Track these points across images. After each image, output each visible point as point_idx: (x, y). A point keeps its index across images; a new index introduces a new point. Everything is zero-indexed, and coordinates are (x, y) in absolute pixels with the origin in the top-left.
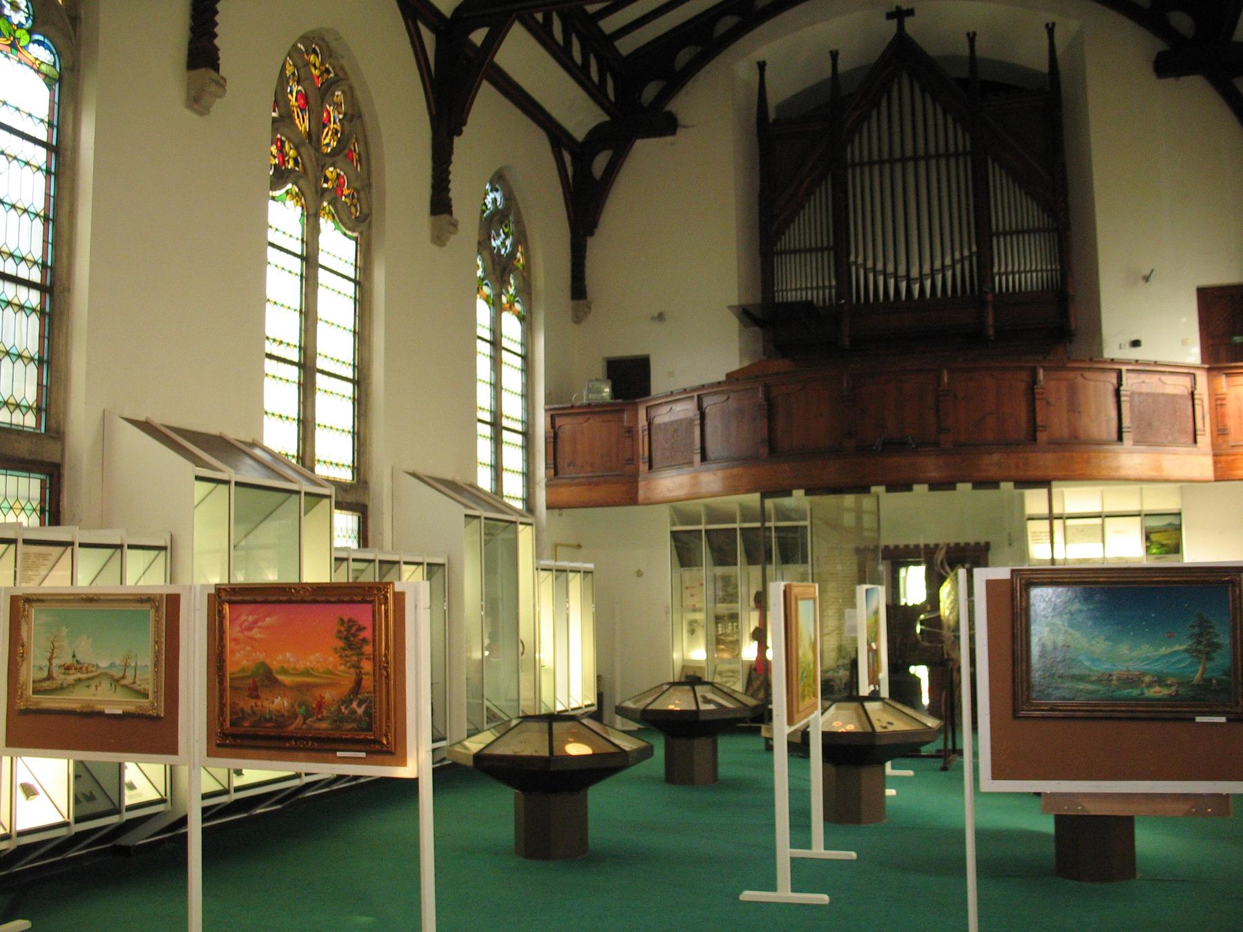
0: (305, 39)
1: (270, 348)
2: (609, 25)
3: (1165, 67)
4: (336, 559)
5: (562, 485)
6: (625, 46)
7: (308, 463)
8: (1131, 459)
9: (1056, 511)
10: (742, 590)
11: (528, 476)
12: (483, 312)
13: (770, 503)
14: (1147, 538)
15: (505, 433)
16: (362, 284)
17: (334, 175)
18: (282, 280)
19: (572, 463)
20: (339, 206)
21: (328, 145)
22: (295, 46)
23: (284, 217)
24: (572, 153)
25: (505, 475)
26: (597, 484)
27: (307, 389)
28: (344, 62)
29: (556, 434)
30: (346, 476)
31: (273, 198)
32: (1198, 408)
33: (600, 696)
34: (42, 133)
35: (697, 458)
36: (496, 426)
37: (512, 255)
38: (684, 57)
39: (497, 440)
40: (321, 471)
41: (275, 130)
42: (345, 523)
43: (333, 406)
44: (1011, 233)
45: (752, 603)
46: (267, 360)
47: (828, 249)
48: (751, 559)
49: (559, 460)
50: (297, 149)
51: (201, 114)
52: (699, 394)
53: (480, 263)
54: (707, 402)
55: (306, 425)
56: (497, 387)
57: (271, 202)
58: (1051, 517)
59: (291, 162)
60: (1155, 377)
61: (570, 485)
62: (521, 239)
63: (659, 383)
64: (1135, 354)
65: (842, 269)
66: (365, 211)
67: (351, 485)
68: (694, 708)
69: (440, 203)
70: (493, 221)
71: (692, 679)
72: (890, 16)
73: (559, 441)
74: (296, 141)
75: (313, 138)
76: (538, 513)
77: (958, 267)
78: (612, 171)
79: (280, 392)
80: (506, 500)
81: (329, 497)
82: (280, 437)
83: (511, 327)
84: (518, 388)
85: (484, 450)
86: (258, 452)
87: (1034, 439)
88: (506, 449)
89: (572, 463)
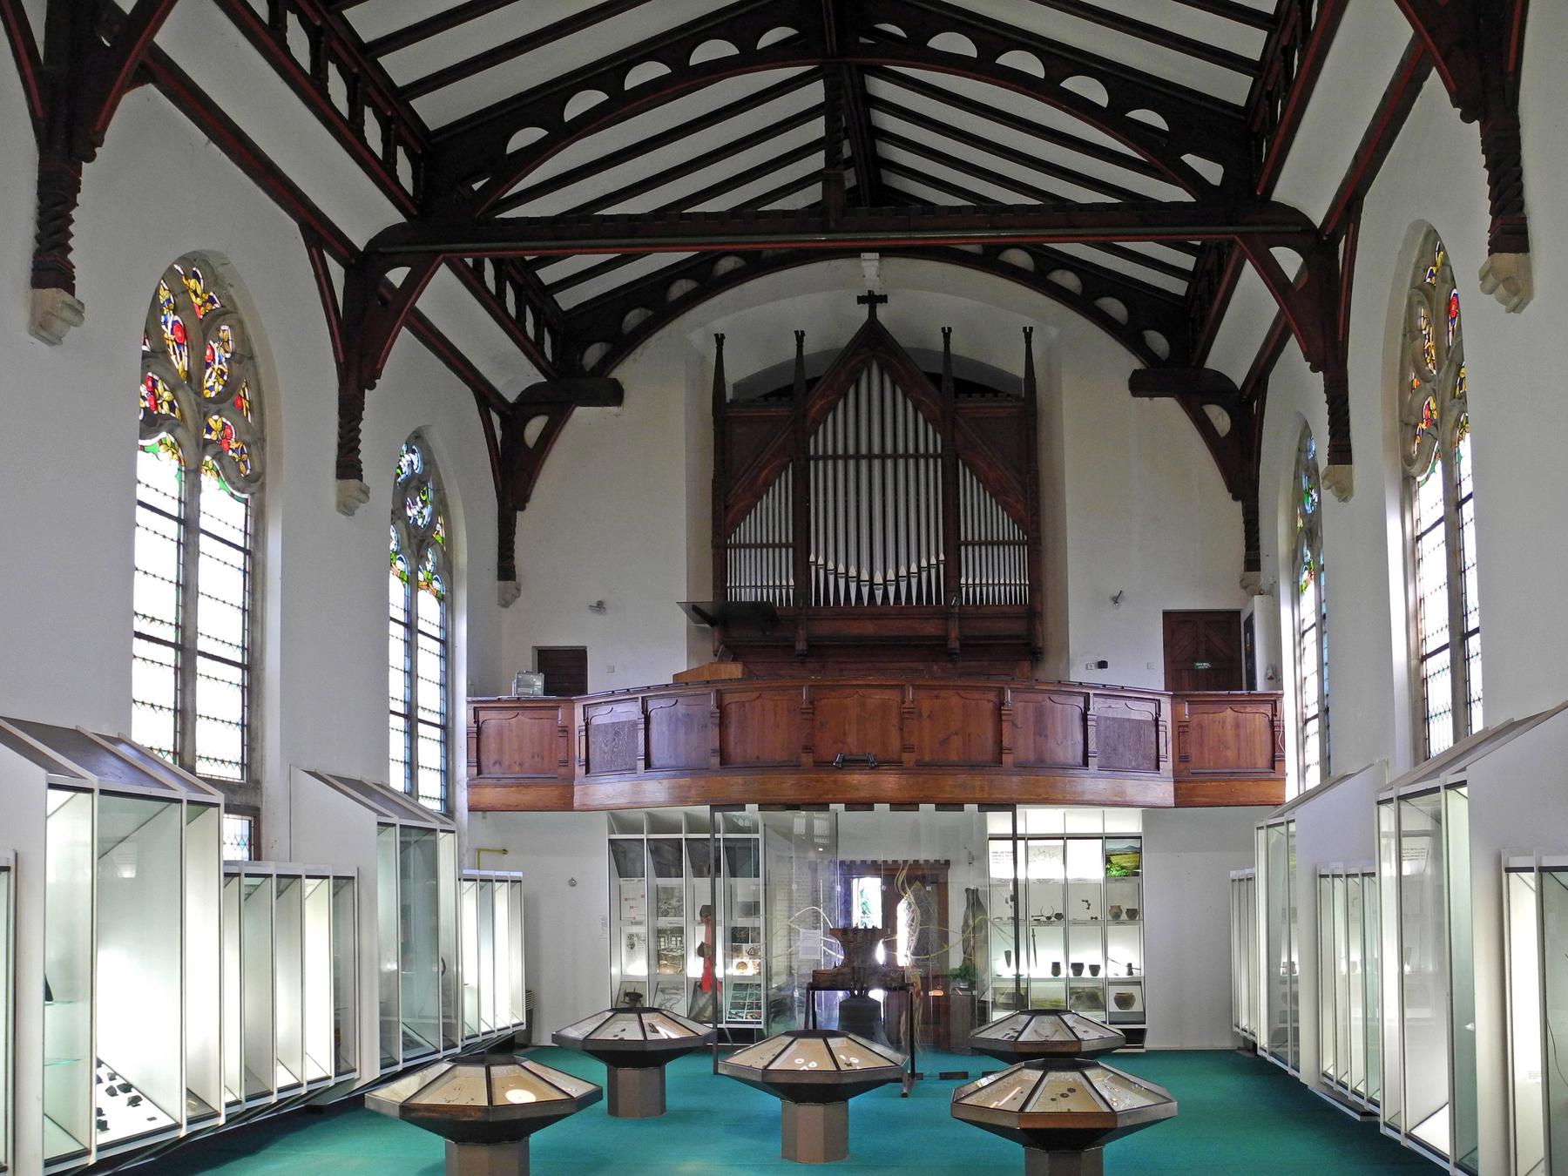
0: (182, 260)
1: (140, 625)
2: (548, 275)
3: (1140, 385)
4: (226, 875)
5: (486, 786)
6: (567, 300)
7: (187, 759)
8: (1093, 783)
9: (1020, 830)
10: (686, 905)
11: (447, 774)
12: (397, 592)
13: (718, 815)
14: (1108, 860)
15: (420, 725)
16: (253, 553)
17: (219, 425)
18: (154, 548)
19: (498, 762)
20: (225, 462)
21: (211, 388)
22: (171, 268)
23: (157, 470)
24: (501, 414)
25: (421, 773)
26: (526, 786)
27: (185, 675)
28: (232, 291)
29: (479, 728)
30: (234, 774)
31: (143, 448)
32: (1162, 735)
33: (530, 1014)
34: (237, 656)
35: (641, 764)
36: (411, 717)
37: (431, 526)
38: (633, 318)
39: (412, 735)
40: (203, 768)
41: (146, 367)
42: (235, 828)
43: (219, 695)
44: (980, 544)
45: (698, 918)
46: (136, 640)
47: (787, 546)
48: (698, 873)
49: (483, 758)
50: (172, 391)
51: (51, 343)
52: (645, 696)
53: (393, 534)
54: (651, 705)
55: (185, 715)
56: (411, 674)
57: (140, 453)
58: (1014, 838)
59: (166, 406)
60: (1122, 702)
61: (496, 786)
62: (441, 507)
63: (597, 681)
64: (1100, 677)
65: (802, 567)
66: (258, 468)
67: (240, 786)
68: (641, 1038)
69: (348, 466)
70: (409, 487)
71: (631, 1002)
72: (861, 300)
73: (483, 738)
74: (172, 381)
75: (194, 379)
76: (458, 815)
77: (924, 575)
78: (548, 438)
79: (152, 678)
80: (421, 801)
81: (217, 805)
82: (152, 730)
83: (429, 609)
84: (436, 676)
85: (397, 745)
86: (123, 749)
87: (999, 761)
88: (422, 744)
89: (498, 762)
